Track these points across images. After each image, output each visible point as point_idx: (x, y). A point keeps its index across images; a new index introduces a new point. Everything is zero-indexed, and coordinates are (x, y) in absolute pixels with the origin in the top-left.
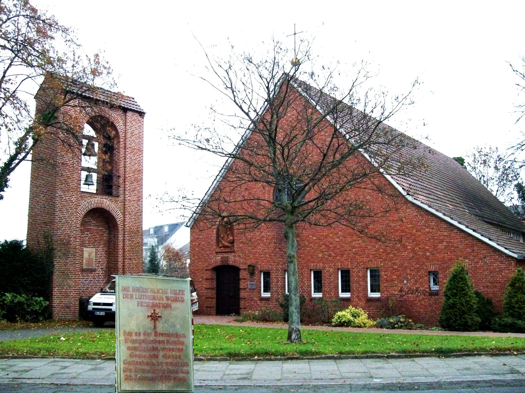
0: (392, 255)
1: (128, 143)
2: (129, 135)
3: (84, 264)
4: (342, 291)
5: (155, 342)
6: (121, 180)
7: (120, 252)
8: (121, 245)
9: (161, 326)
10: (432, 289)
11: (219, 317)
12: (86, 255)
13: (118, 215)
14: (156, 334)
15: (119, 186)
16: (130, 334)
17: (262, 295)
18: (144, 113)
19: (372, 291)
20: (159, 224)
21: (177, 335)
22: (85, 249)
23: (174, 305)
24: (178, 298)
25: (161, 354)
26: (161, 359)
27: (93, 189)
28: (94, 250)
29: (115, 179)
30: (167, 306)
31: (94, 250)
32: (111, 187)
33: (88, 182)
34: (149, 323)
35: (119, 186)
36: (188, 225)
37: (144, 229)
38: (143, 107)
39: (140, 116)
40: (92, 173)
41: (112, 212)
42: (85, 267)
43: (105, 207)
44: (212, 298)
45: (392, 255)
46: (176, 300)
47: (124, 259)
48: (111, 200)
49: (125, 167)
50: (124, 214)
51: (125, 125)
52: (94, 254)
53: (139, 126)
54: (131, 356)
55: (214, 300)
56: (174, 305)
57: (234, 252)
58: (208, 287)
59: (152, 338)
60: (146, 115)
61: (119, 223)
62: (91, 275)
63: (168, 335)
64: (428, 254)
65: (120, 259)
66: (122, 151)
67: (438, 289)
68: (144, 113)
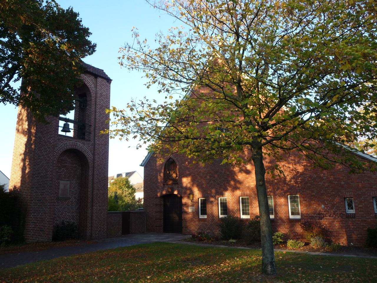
0: (309, 185)
1: (98, 101)
2: (99, 95)
3: (60, 193)
4: (201, 214)
6: (92, 128)
7: (90, 184)
8: (90, 179)
10: (347, 212)
11: (167, 235)
12: (61, 186)
13: (89, 155)
15: (91, 133)
17: (200, 217)
18: (111, 80)
19: (243, 214)
20: (119, 173)
22: (61, 182)
27: (71, 134)
28: (69, 182)
29: (87, 128)
31: (69, 182)
32: (84, 134)
33: (66, 129)
35: (91, 133)
36: (142, 165)
37: (109, 176)
38: (110, 76)
39: (108, 82)
40: (69, 123)
41: (84, 153)
44: (160, 219)
45: (309, 185)
47: (93, 189)
48: (83, 144)
49: (95, 119)
50: (94, 155)
51: (96, 87)
52: (69, 185)
53: (107, 90)
55: (162, 221)
57: (177, 184)
58: (157, 211)
60: (112, 82)
61: (89, 161)
64: (343, 183)
65: (90, 189)
66: (93, 107)
67: (354, 213)
68: (111, 80)
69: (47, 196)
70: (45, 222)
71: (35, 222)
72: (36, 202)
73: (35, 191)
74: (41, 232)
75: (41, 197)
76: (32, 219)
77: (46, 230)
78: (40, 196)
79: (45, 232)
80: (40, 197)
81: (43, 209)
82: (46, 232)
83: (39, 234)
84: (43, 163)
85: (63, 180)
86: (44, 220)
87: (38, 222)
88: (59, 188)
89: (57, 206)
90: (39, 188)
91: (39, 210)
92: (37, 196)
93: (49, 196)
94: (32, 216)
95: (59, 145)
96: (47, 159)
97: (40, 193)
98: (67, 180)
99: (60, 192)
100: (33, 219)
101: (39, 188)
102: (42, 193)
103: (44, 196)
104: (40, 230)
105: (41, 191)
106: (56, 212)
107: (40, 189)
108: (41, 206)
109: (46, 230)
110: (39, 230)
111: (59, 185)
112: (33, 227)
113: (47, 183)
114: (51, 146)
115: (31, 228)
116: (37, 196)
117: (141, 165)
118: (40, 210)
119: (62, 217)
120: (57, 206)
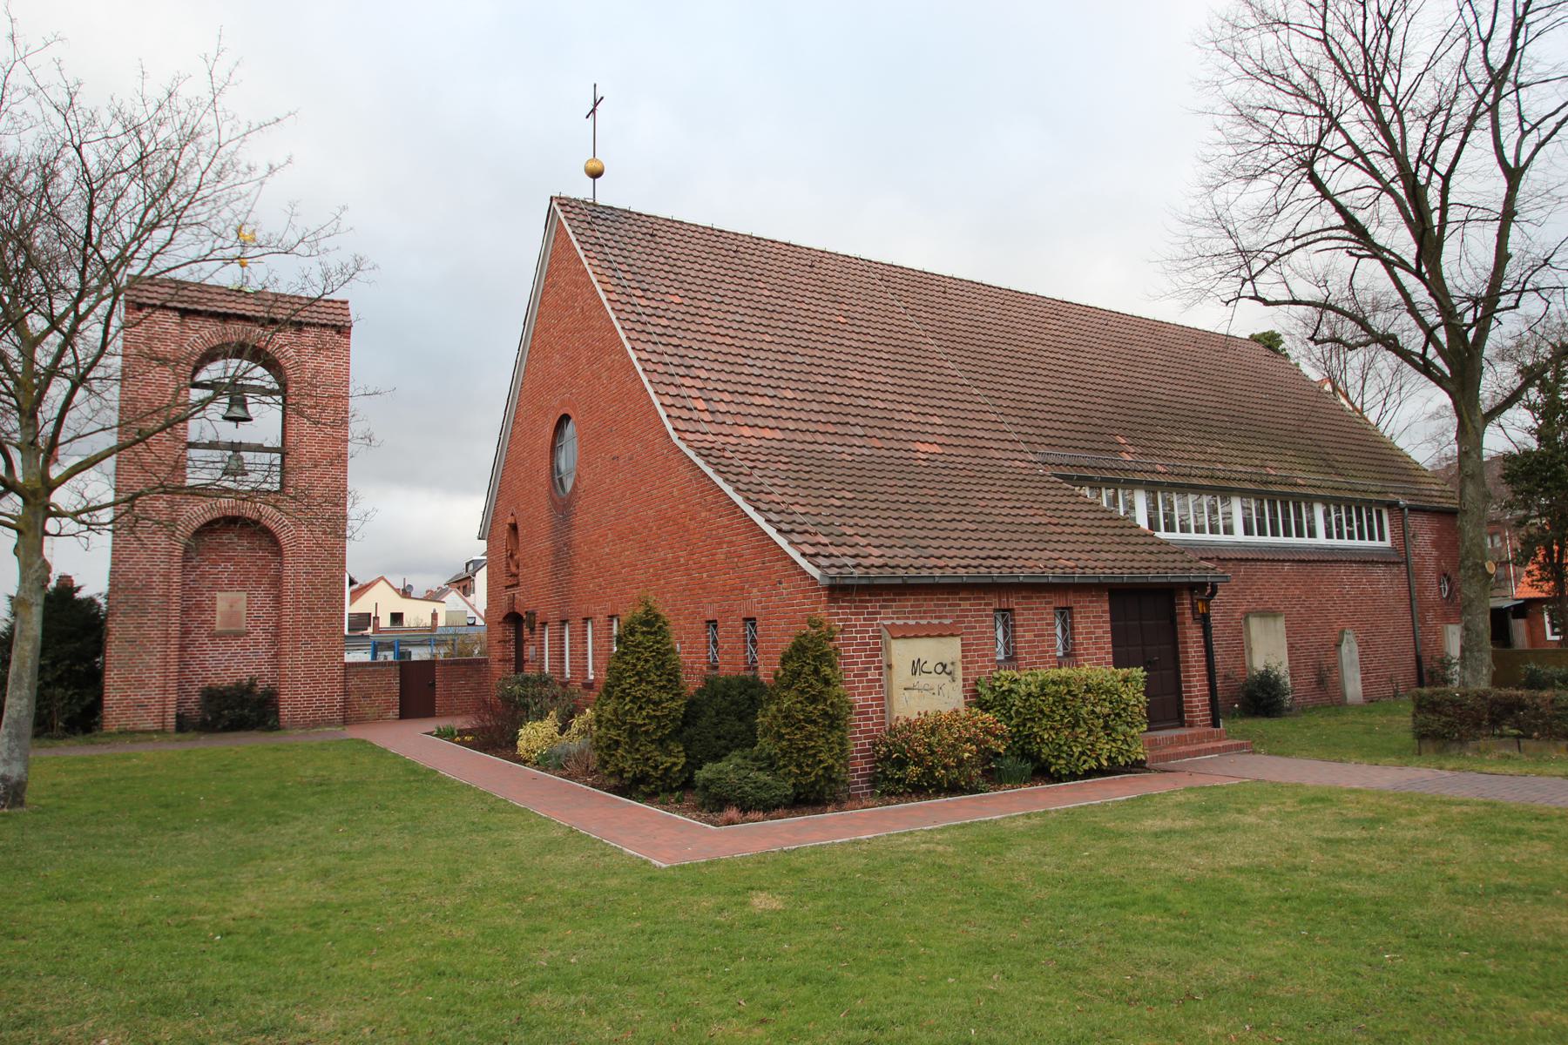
22: (219, 595)
28: (244, 595)
31: (244, 595)
42: (218, 628)
52: (244, 603)
62: (235, 645)
99: (218, 618)
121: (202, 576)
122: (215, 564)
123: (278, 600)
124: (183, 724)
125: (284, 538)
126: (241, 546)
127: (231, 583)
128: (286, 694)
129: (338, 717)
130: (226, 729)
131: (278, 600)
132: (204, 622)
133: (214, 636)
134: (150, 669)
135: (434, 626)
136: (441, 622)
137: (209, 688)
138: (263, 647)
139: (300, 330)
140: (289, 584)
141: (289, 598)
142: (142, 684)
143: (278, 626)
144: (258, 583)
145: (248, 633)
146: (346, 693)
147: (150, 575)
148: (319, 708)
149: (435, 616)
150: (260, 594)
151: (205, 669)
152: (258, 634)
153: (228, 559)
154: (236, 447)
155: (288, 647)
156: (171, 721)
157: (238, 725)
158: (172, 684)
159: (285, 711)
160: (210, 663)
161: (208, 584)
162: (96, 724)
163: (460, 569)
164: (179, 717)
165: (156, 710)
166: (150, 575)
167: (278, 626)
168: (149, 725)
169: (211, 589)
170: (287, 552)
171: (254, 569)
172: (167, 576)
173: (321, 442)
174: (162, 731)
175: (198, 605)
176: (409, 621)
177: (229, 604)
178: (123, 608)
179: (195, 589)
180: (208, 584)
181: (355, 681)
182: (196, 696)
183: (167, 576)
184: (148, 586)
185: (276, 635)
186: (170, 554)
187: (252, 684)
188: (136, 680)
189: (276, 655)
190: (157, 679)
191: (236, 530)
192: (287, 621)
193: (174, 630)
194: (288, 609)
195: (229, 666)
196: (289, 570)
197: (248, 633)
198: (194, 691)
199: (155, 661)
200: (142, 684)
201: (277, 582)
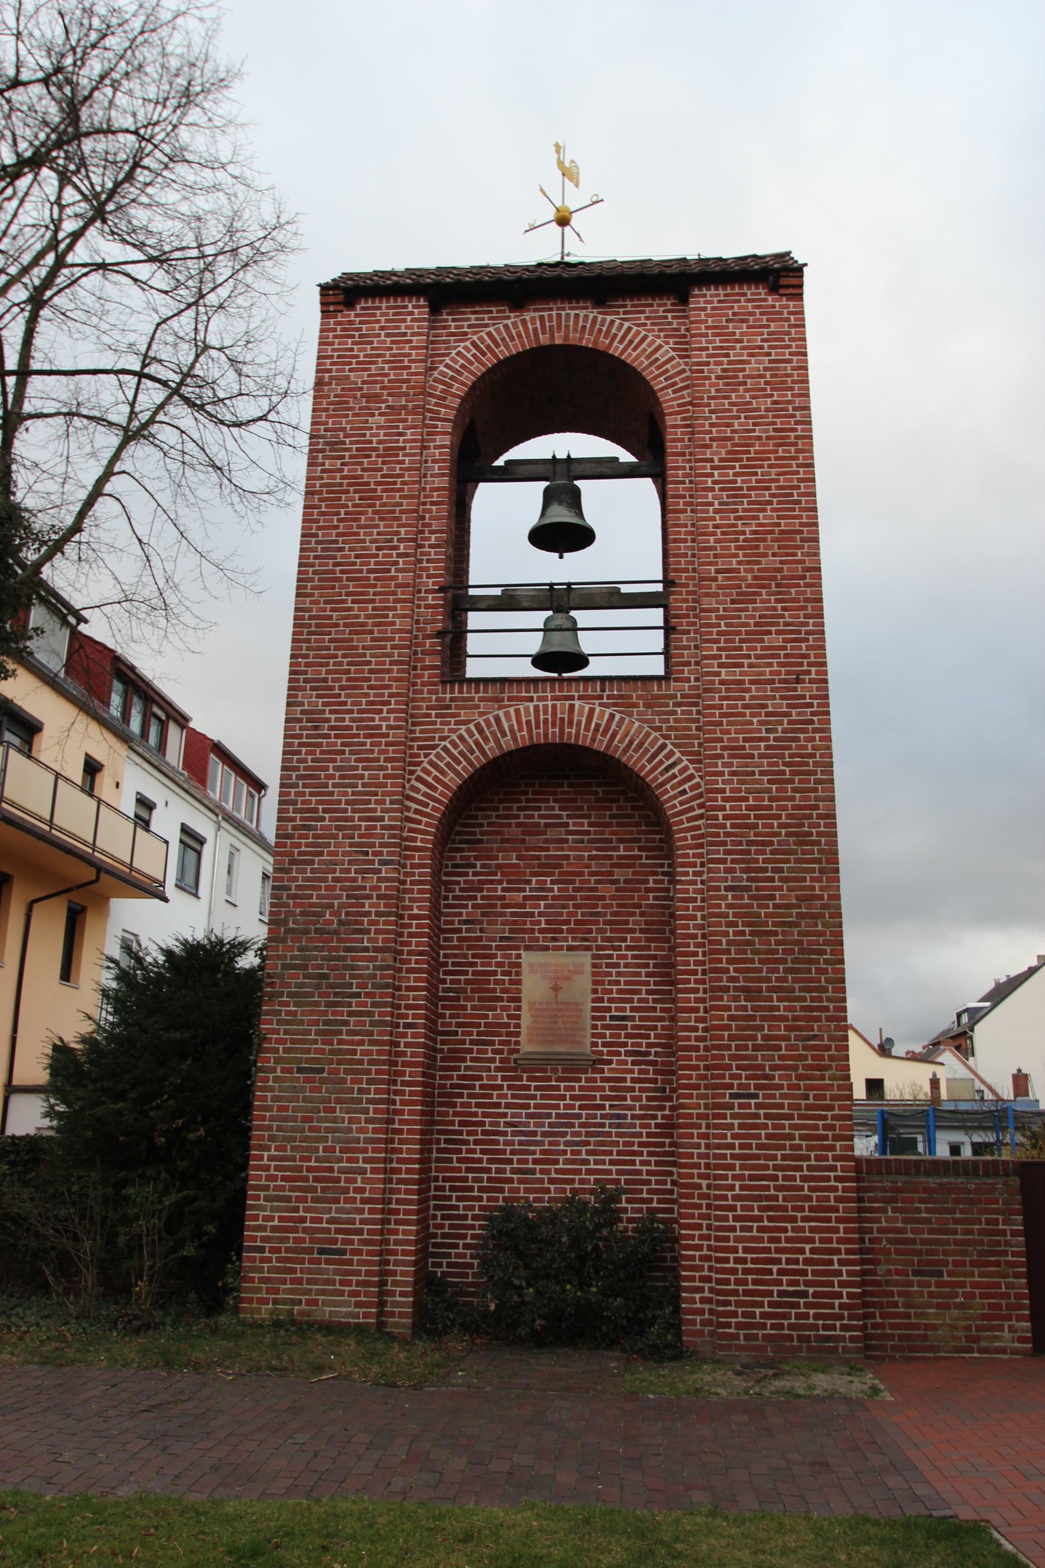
3: (524, 1030)
5: (556, 1010)
9: (562, 996)
12: (534, 987)
14: (557, 1003)
16: (534, 1003)
21: (576, 1004)
22: (527, 958)
23: (574, 977)
24: (578, 970)
25: (560, 1020)
26: (560, 1025)
28: (585, 959)
30: (567, 978)
31: (585, 959)
34: (551, 994)
41: (539, 736)
42: (527, 1046)
43: (585, 739)
46: (577, 972)
52: (585, 981)
54: (534, 1022)
56: (574, 977)
59: (553, 1006)
62: (568, 1092)
63: (568, 1004)
69: (361, 1043)
70: (353, 1200)
71: (288, 1199)
72: (293, 1080)
73: (288, 1013)
74: (328, 1262)
75: (322, 1051)
76: (269, 1178)
77: (359, 1252)
78: (316, 1042)
79: (350, 1262)
80: (316, 1051)
81: (334, 1120)
82: (361, 1263)
83: (310, 1271)
84: (336, 854)
85: (546, 948)
86: (346, 1190)
87: (304, 1200)
88: (518, 1000)
89: (508, 1106)
90: (312, 995)
91: (312, 1129)
92: (299, 1041)
93: (372, 1043)
94: (271, 1158)
95: (442, 739)
96: (359, 827)
97: (316, 1023)
98: (571, 948)
99: (526, 1021)
100: (274, 1178)
101: (312, 995)
102: (326, 1023)
103: (341, 1042)
104: (321, 1251)
105: (325, 1013)
106: (511, 1143)
107: (317, 1004)
108: (323, 1100)
109: (359, 1252)
110: (310, 1251)
111: (519, 982)
112: (274, 1229)
113: (358, 968)
114: (381, 752)
115: (263, 1229)
116: (299, 1041)
117: (561, 557)
118: (317, 1129)
119: (552, 1181)
120: (508, 1106)
121: (488, 909)
122: (517, 881)
123: (667, 972)
124: (438, 1308)
125: (672, 801)
126: (569, 829)
127: (554, 929)
128: (695, 1247)
129: (845, 1333)
130: (539, 1341)
131: (667, 972)
132: (494, 1028)
133: (517, 1068)
134: (350, 1149)
135: (936, 1098)
136: (944, 1094)
137: (508, 1212)
138: (635, 1103)
139: (683, 299)
140: (692, 923)
141: (692, 960)
142: (331, 1189)
143: (670, 1044)
144: (620, 927)
145: (597, 1063)
146: (866, 1254)
147: (357, 896)
148: (789, 1300)
149: (935, 1083)
150: (91, 213)
151: (497, 1157)
152: (622, 1065)
153: (548, 867)
154: (560, 600)
155: (695, 1104)
156: (401, 1300)
157: (573, 1329)
158: (406, 1195)
159: (696, 1299)
160: (508, 1141)
161: (500, 929)
162: (228, 1290)
163: (947, 1021)
164: (428, 1284)
165: (363, 1264)
166: (357, 896)
167: (670, 1044)
168: (345, 1307)
169: (508, 944)
170: (687, 851)
171: (607, 890)
172: (396, 899)
173: (751, 546)
174: (376, 1333)
175: (480, 983)
176: (892, 1091)
177: (552, 983)
178: (296, 980)
179: (472, 943)
180: (500, 929)
181: (887, 1218)
182: (475, 1229)
183: (396, 899)
184: (353, 925)
185: (666, 1076)
186: (404, 847)
187: (609, 1198)
188: (323, 1185)
189: (669, 1127)
190: (367, 1182)
191: (556, 780)
192: (692, 1029)
193: (412, 1042)
194: (692, 994)
195: (552, 1152)
196: (689, 882)
197: (597, 1063)
198: (472, 1215)
199: (364, 1129)
200: (331, 1189)
201: (663, 925)
